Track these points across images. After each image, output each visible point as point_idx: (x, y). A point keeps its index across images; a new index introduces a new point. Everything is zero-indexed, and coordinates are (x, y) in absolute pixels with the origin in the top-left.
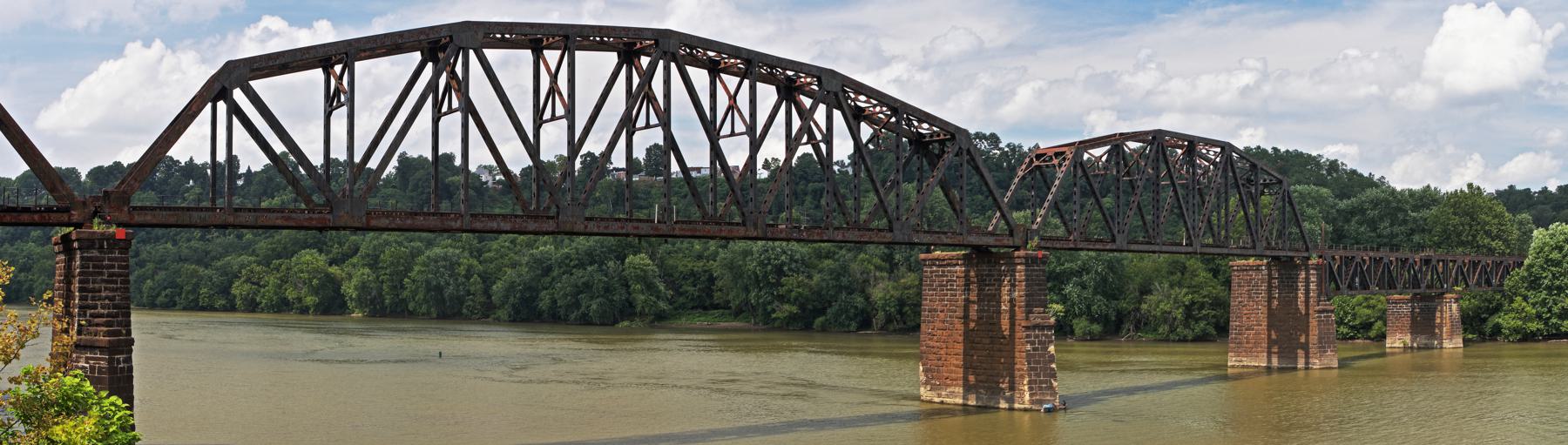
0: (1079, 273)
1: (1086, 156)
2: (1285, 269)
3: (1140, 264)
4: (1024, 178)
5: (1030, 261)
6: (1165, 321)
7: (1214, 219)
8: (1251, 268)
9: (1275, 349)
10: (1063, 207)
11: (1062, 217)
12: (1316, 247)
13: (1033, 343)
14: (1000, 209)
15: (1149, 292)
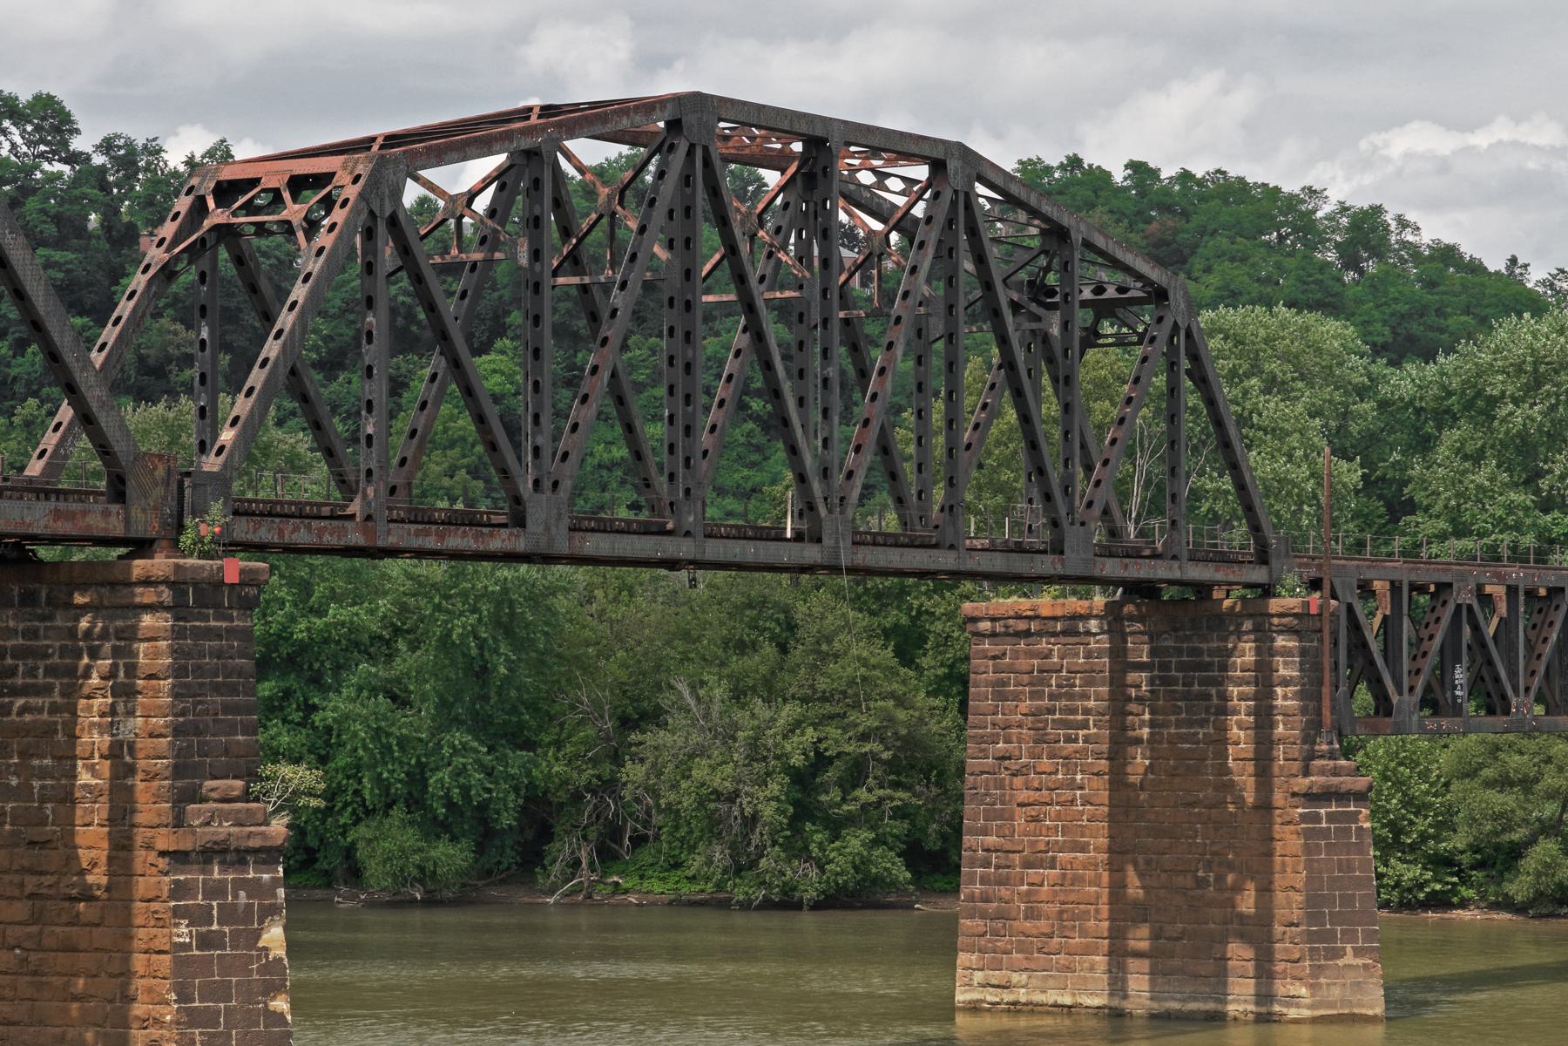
0: (380, 646)
1: (412, 193)
2: (1177, 626)
3: (608, 610)
4: (168, 273)
5: (193, 598)
6: (714, 828)
7: (904, 438)
8: (1046, 626)
9: (1140, 939)
10: (325, 391)
11: (317, 426)
12: (1294, 546)
13: (198, 917)
14: (71, 390)
15: (654, 717)
